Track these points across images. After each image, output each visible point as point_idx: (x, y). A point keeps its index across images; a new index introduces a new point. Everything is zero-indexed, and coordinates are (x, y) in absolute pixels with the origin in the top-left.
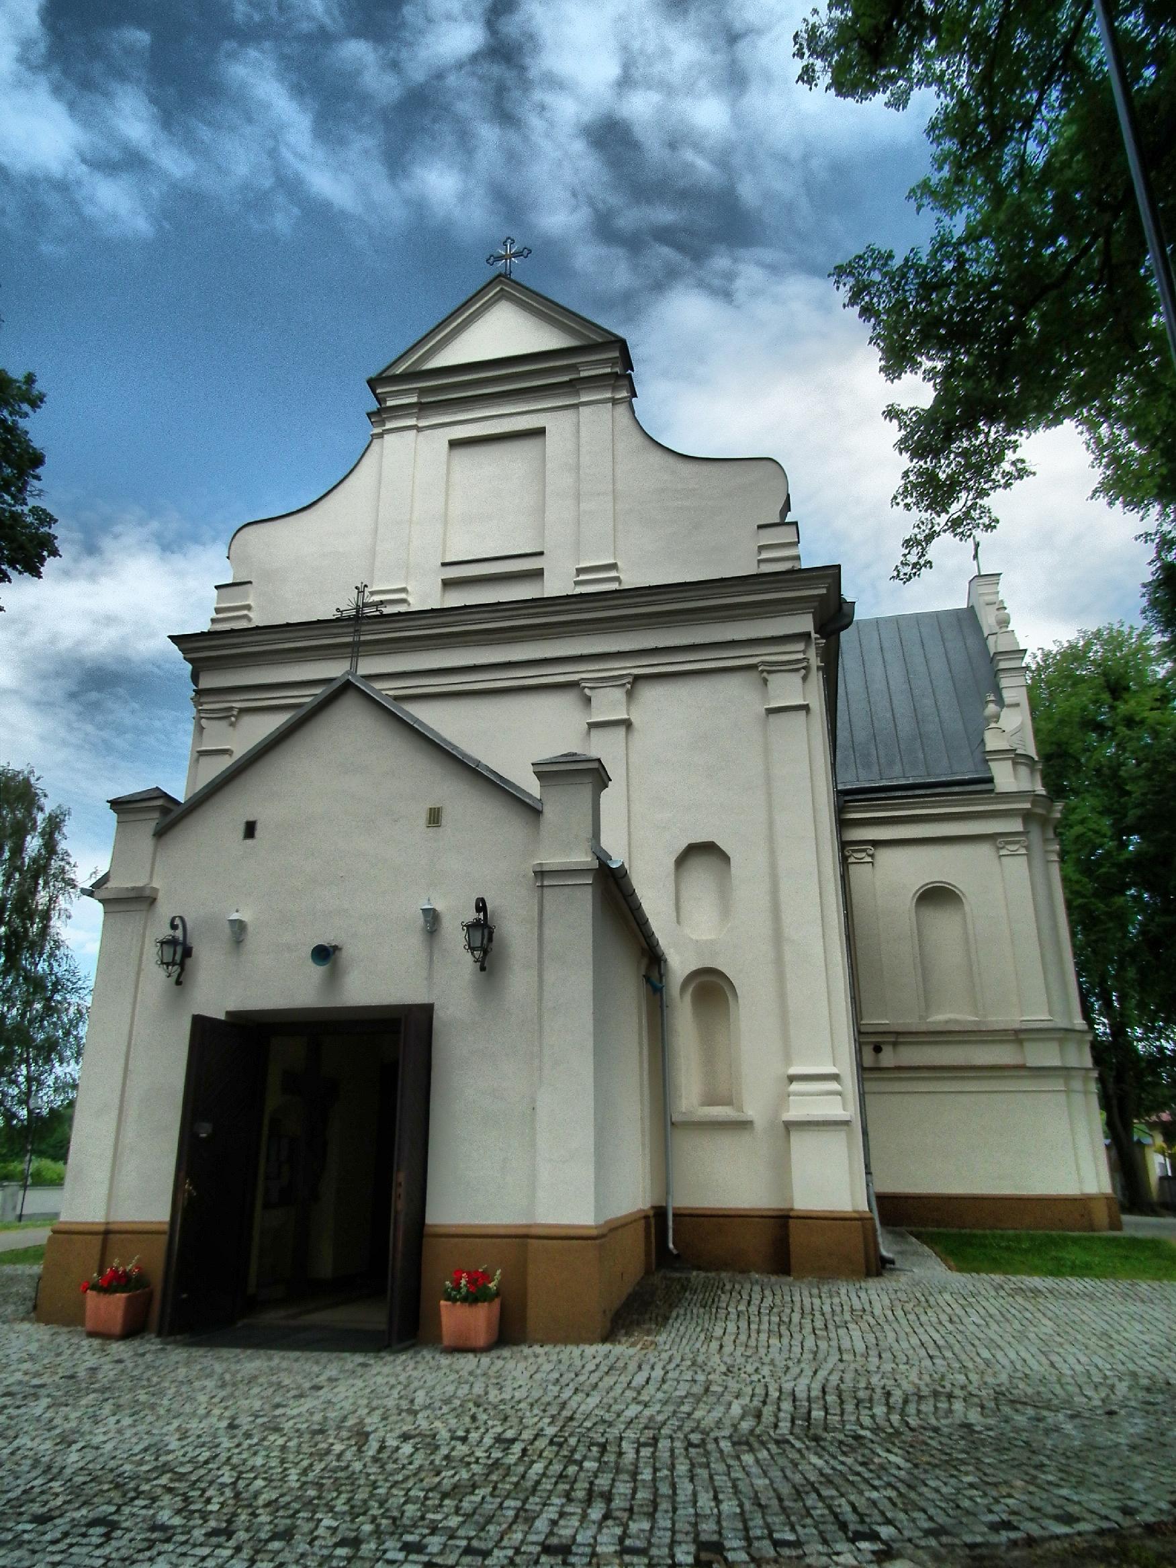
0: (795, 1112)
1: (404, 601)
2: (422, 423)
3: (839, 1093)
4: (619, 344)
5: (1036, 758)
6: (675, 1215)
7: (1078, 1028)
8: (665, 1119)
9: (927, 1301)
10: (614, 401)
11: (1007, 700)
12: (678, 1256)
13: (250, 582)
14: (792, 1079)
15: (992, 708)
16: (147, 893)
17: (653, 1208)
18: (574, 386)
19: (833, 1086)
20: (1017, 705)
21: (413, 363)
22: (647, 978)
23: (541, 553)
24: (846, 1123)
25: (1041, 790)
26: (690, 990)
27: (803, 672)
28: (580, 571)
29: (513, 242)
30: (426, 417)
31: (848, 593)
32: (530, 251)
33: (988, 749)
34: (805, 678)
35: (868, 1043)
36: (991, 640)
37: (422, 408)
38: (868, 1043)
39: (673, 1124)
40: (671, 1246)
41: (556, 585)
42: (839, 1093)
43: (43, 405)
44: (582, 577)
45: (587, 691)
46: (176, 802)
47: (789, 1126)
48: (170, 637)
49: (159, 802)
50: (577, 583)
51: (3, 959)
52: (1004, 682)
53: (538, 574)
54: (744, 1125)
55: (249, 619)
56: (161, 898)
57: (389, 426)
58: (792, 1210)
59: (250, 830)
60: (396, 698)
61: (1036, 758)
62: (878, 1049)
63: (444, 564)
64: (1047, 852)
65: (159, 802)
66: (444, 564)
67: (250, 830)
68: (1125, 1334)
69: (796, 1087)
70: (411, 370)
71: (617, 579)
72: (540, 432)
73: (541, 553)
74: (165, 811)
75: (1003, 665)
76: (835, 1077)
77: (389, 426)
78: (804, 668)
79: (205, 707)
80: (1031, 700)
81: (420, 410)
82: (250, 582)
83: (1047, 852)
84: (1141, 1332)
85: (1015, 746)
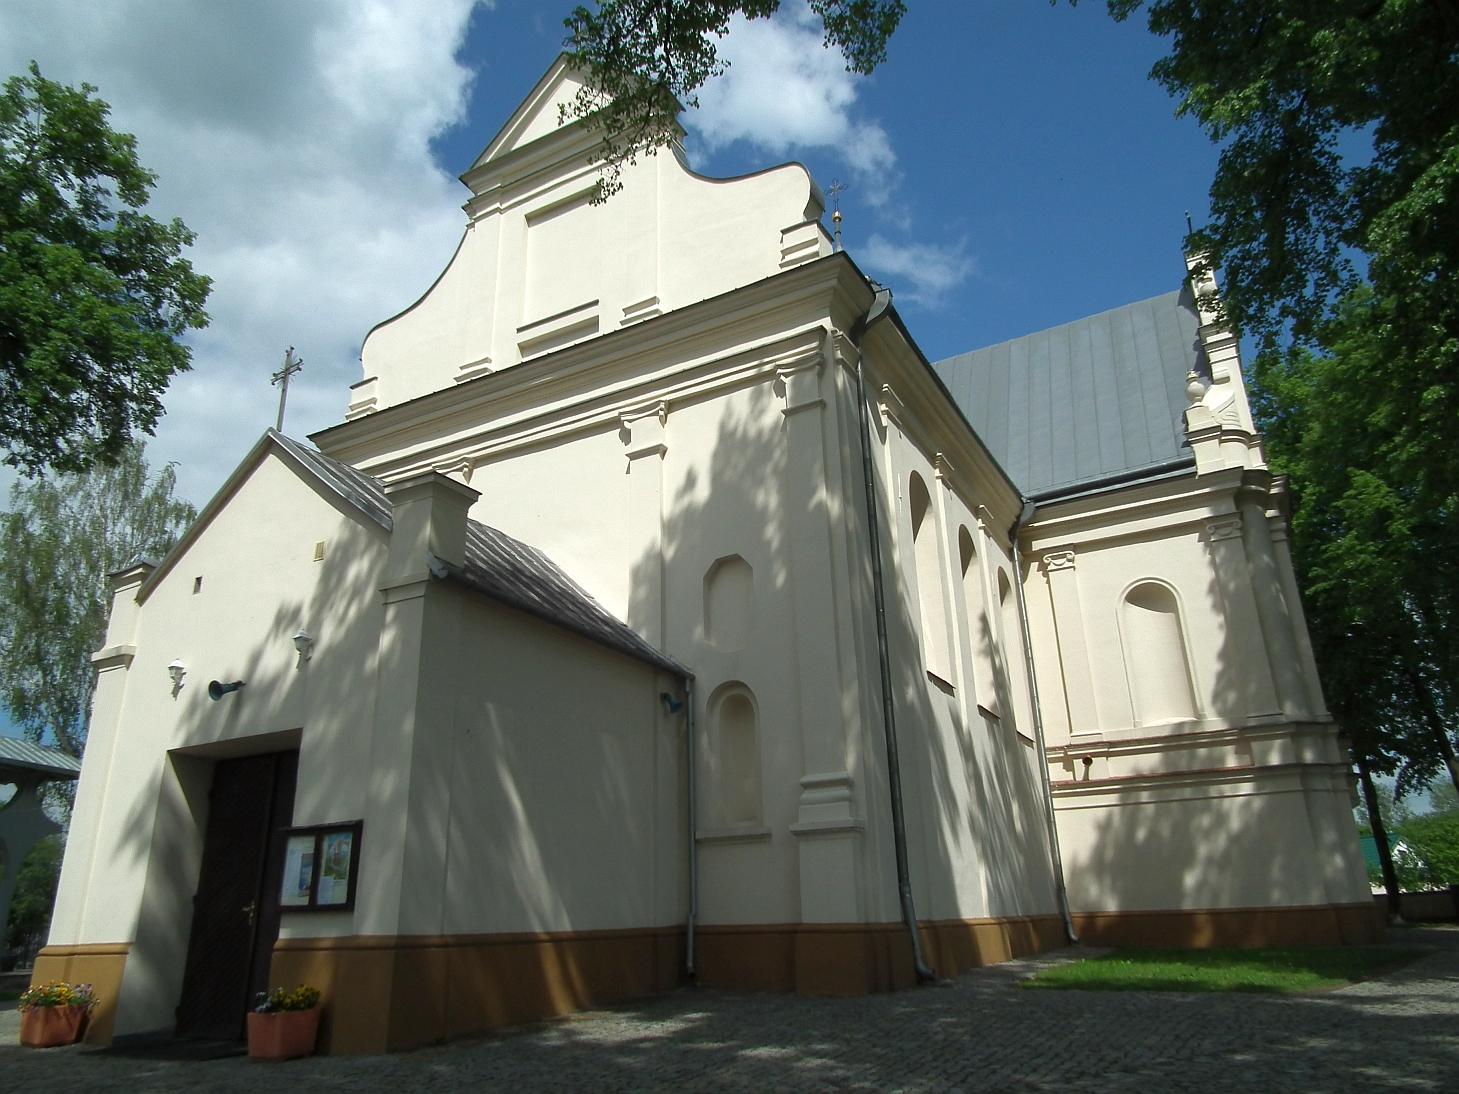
0: (804, 822)
6: (696, 934)
7: (1321, 720)
8: (689, 835)
11: (1216, 376)
12: (692, 976)
13: (375, 378)
19: (844, 791)
20: (1226, 380)
26: (718, 708)
31: (207, 298)
35: (1077, 757)
37: (505, 192)
38: (1077, 757)
42: (849, 799)
45: (626, 423)
48: (307, 437)
49: (140, 570)
52: (1214, 356)
53: (594, 323)
54: (764, 837)
56: (664, 692)
57: (478, 215)
61: (1253, 432)
62: (1088, 761)
64: (1272, 531)
65: (140, 570)
69: (808, 795)
70: (503, 154)
73: (596, 303)
75: (1210, 340)
77: (478, 215)
81: (503, 194)
82: (375, 378)
83: (1272, 531)
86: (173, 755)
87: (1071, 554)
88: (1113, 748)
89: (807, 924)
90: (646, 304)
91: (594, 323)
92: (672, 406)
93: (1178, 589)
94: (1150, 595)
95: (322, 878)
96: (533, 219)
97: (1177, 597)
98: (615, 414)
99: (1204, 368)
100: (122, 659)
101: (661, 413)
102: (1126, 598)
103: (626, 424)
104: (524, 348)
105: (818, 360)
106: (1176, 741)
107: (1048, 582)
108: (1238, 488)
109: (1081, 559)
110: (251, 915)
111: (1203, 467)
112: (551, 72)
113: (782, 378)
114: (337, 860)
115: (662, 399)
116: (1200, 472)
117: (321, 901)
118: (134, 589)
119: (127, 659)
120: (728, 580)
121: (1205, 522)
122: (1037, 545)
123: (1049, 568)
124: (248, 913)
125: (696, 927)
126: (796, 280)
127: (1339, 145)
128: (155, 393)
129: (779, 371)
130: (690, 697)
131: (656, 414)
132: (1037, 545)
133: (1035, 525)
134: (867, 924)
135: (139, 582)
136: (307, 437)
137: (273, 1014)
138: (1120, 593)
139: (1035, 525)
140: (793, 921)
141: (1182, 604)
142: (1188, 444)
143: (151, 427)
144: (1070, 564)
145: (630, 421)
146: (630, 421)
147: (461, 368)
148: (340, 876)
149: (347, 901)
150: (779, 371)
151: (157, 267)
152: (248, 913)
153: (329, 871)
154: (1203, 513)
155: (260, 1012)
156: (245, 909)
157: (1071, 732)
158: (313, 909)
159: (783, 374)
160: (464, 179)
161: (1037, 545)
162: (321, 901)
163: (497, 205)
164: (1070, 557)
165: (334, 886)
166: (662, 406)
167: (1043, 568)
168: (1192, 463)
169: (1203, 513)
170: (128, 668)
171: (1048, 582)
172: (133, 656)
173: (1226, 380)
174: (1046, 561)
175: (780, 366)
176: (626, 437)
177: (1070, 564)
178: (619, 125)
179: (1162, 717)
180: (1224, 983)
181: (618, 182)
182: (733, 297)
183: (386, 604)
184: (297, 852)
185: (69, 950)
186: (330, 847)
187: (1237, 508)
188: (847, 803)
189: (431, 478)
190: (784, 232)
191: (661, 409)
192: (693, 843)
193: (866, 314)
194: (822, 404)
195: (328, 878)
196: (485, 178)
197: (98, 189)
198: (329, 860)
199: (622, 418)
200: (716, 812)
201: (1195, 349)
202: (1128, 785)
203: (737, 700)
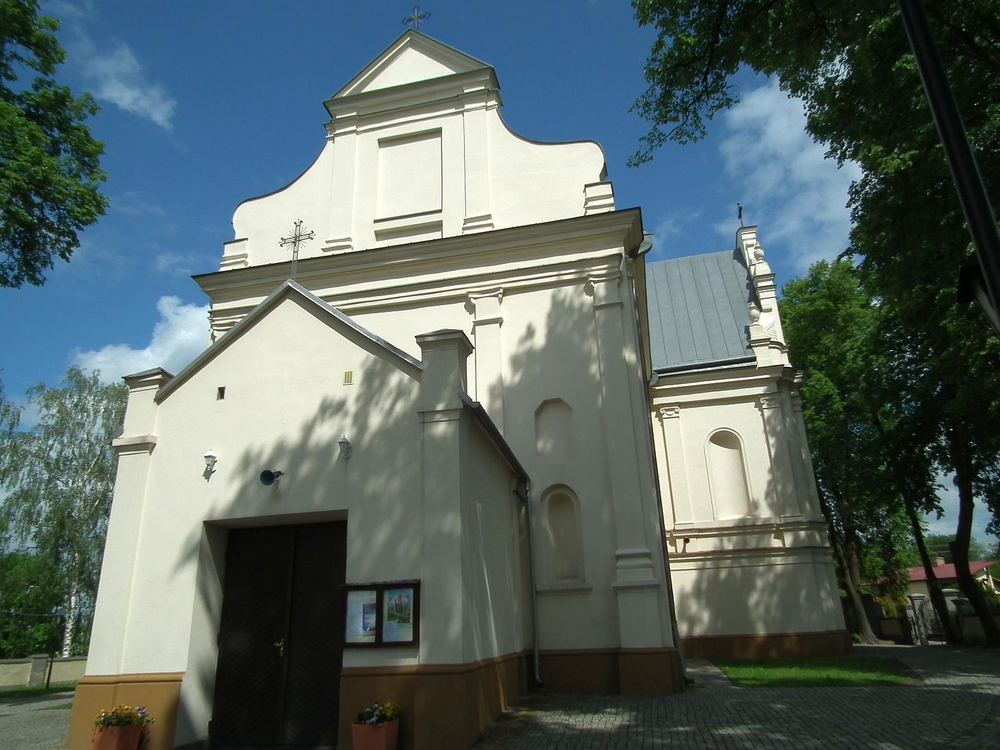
1: (349, 246)
2: (360, 129)
3: (651, 566)
4: (489, 71)
5: (784, 344)
9: (713, 708)
10: (487, 108)
11: (764, 307)
12: (542, 685)
13: (247, 239)
14: (618, 557)
15: (755, 312)
16: (149, 440)
17: (524, 651)
18: (460, 100)
19: (646, 561)
20: (770, 310)
21: (356, 88)
22: (517, 492)
23: (440, 211)
24: (657, 586)
25: (787, 364)
26: (547, 499)
27: (618, 280)
28: (466, 221)
29: (419, 9)
30: (361, 126)
32: (430, 15)
33: (611, 193)
34: (619, 285)
36: (752, 268)
37: (360, 120)
39: (537, 592)
40: (537, 677)
41: (453, 228)
42: (651, 566)
43: (34, 82)
44: (468, 225)
45: (472, 300)
46: (171, 377)
47: (618, 590)
48: (192, 277)
49: (159, 377)
50: (464, 229)
51: (883, 745)
52: (762, 295)
53: (438, 226)
55: (247, 263)
57: (337, 132)
58: (620, 648)
59: (221, 392)
60: (344, 311)
61: (784, 344)
62: (686, 541)
63: (375, 221)
65: (159, 377)
66: (375, 221)
67: (221, 392)
68: (851, 726)
69: (621, 563)
70: (355, 93)
71: (491, 225)
72: (437, 132)
73: (440, 211)
74: (161, 383)
75: (760, 284)
76: (648, 555)
77: (337, 132)
78: (618, 278)
79: (216, 323)
80: (780, 307)
82: (247, 239)
84: (863, 724)
85: (770, 336)
86: (204, 522)
87: (677, 409)
88: (701, 533)
89: (625, 649)
90: (485, 218)
91: (438, 226)
92: (507, 292)
93: (742, 436)
94: (724, 439)
95: (386, 622)
96: (383, 143)
97: (739, 437)
98: (464, 292)
99: (755, 298)
100: (145, 446)
101: (501, 296)
102: (710, 440)
103: (473, 300)
104: (380, 235)
105: (618, 275)
106: (742, 528)
107: (662, 425)
108: (780, 378)
109: (683, 412)
110: (282, 649)
111: (761, 362)
112: (401, 40)
113: (592, 283)
114: (400, 608)
115: (501, 286)
116: (758, 366)
117: (385, 639)
118: (153, 391)
119: (150, 446)
120: (551, 414)
121: (760, 396)
122: (657, 401)
123: (664, 416)
124: (280, 647)
125: (539, 651)
126: (598, 221)
127: (654, 158)
128: (73, 228)
129: (591, 279)
130: (528, 493)
131: (496, 296)
132: (657, 401)
133: (657, 388)
134: (665, 648)
135: (157, 386)
136: (192, 277)
137: (380, 724)
138: (706, 437)
139: (657, 388)
140: (612, 646)
141: (744, 445)
142: (750, 347)
143: (67, 255)
144: (677, 415)
145: (475, 298)
146: (475, 298)
147: (327, 242)
148: (404, 620)
149: (414, 638)
150: (591, 279)
151: (64, 126)
152: (280, 647)
153: (391, 617)
154: (760, 390)
155: (370, 724)
156: (278, 645)
157: (675, 521)
158: (379, 644)
159: (593, 281)
160: (326, 104)
161: (657, 401)
162: (385, 639)
163: (354, 128)
164: (676, 410)
165: (398, 628)
166: (501, 291)
167: (659, 416)
168: (754, 359)
169: (760, 390)
170: (151, 453)
171: (662, 425)
172: (155, 444)
173: (770, 310)
174: (661, 412)
175: (592, 276)
176: (471, 308)
177: (677, 415)
178: (688, 128)
179: (730, 515)
180: (909, 678)
181: (650, 156)
182: (558, 225)
183: (424, 423)
184: (358, 603)
185: (115, 679)
186: (390, 599)
187: (778, 389)
188: (650, 569)
189: (459, 336)
190: (586, 186)
191: (500, 293)
192: (532, 594)
193: (638, 248)
194: (621, 305)
195: (392, 622)
196: (344, 106)
197: (15, 56)
198: (390, 609)
199: (470, 296)
200: (548, 572)
201: (747, 288)
202: (718, 555)
203: (561, 496)
